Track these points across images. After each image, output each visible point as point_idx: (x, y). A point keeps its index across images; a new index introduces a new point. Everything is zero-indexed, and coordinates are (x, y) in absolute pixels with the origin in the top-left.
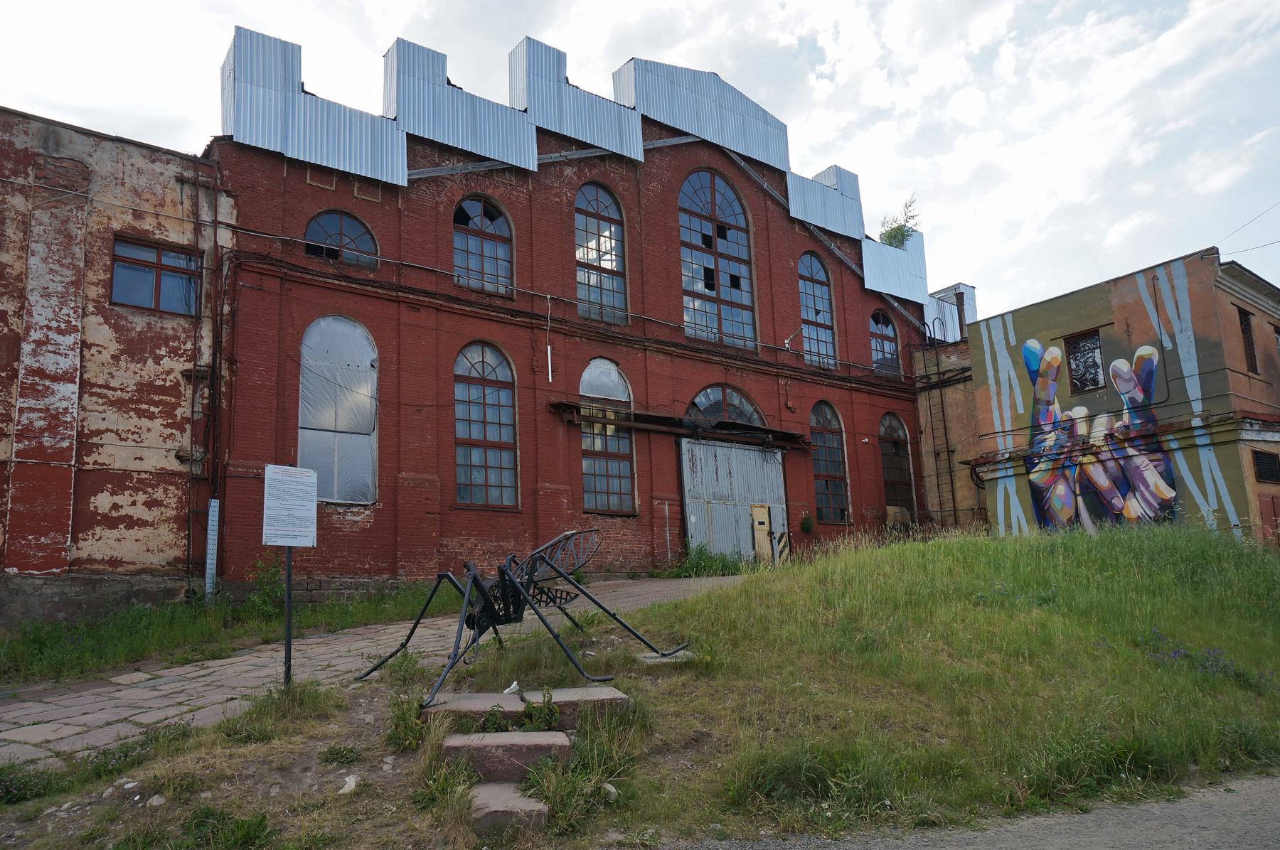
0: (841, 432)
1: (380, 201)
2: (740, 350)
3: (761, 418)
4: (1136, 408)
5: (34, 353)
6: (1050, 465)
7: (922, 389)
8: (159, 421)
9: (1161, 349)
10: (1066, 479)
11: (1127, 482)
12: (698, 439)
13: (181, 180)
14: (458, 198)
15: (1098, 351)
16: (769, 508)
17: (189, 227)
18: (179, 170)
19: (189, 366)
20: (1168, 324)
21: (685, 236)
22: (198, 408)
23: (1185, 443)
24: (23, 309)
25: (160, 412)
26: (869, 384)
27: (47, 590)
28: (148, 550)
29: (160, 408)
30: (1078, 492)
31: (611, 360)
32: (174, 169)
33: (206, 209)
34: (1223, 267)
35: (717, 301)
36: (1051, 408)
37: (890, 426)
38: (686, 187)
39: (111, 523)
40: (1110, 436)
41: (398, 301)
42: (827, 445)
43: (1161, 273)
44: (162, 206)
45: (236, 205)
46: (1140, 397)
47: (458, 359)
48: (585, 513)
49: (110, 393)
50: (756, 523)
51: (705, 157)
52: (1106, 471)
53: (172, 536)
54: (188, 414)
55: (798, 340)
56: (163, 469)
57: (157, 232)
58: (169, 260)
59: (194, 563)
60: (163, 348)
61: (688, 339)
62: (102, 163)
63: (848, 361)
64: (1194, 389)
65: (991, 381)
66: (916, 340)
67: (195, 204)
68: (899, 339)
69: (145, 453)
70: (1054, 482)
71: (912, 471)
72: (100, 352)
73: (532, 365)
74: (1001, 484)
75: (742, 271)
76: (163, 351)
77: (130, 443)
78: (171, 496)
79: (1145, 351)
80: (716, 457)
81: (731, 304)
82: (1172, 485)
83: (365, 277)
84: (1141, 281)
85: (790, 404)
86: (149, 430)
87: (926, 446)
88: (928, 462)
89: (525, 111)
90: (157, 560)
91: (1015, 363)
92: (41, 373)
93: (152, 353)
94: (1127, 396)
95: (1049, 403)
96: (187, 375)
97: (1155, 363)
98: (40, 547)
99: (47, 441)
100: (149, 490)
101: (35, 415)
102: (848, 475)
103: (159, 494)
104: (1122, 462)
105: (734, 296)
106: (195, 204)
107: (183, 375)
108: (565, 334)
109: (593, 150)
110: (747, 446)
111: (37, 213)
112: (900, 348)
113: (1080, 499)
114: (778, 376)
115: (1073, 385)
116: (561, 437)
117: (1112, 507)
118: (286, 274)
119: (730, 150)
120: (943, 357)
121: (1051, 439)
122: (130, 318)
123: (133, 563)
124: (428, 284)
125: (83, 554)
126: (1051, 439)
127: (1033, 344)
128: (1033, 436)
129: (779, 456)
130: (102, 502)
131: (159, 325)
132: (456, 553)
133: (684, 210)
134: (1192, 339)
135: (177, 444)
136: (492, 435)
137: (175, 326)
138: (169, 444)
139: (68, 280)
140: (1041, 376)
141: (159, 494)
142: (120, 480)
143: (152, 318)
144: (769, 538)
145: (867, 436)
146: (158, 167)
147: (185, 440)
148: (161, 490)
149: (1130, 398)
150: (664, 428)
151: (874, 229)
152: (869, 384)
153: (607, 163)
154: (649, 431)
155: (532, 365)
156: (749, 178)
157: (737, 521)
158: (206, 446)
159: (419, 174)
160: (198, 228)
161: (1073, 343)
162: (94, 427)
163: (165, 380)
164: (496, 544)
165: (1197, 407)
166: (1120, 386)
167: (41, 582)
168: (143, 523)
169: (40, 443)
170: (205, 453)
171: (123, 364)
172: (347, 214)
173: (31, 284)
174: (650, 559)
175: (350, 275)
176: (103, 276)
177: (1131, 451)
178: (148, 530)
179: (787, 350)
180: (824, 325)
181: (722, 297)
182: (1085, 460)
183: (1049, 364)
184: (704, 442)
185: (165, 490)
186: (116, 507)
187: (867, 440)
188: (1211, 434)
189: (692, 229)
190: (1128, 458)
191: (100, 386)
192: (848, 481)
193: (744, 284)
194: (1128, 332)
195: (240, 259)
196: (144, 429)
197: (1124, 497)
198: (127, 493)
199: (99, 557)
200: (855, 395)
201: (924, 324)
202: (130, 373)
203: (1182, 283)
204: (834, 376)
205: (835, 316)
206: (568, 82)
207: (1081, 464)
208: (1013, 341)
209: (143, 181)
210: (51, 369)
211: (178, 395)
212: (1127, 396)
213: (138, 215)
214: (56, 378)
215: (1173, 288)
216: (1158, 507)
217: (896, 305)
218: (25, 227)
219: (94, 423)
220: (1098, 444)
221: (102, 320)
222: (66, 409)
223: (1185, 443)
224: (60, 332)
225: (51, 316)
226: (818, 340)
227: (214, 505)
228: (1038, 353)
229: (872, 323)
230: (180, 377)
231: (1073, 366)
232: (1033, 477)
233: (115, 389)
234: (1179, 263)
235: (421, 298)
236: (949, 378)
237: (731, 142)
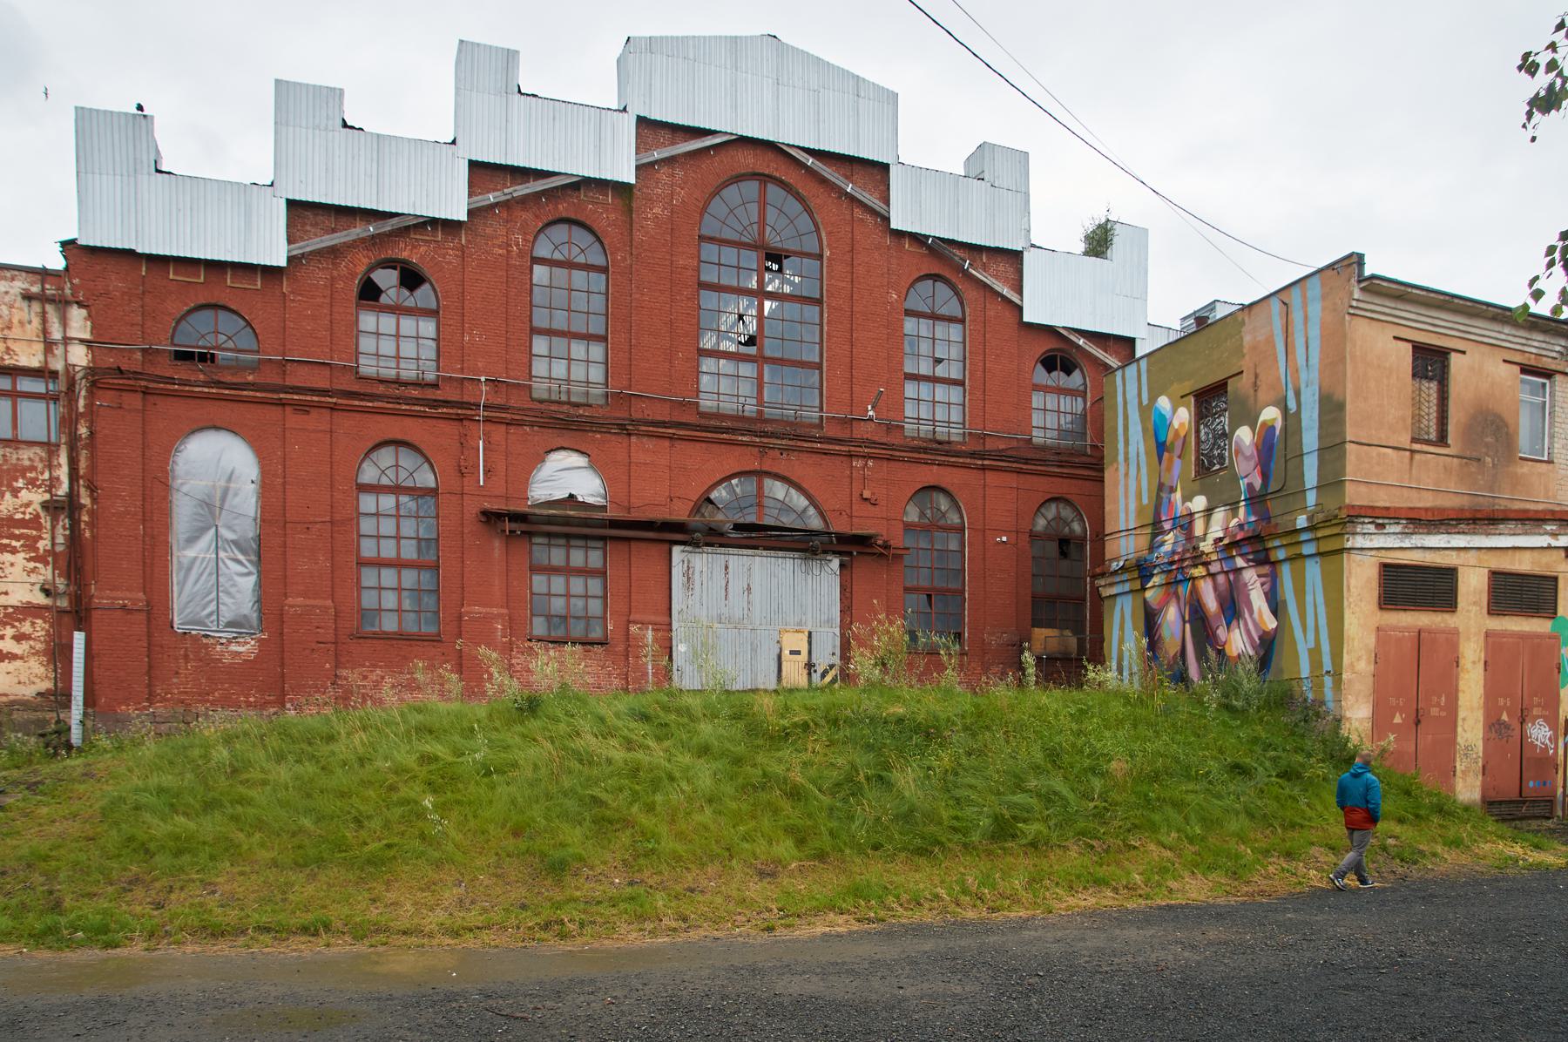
1: (259, 287)
2: (791, 424)
3: (821, 514)
8: (22, 555)
12: (699, 547)
13: (28, 297)
14: (362, 269)
16: (810, 633)
17: (40, 347)
19: (47, 497)
22: (60, 540)
23: (1293, 551)
25: (22, 546)
26: (1017, 460)
28: (19, 683)
29: (22, 542)
30: (1187, 618)
32: (19, 285)
33: (55, 320)
34: (1362, 285)
37: (1058, 518)
41: (282, 404)
42: (936, 547)
44: (9, 328)
45: (90, 317)
47: (365, 465)
50: (786, 652)
51: (748, 160)
53: (43, 669)
54: (49, 547)
56: (29, 603)
57: (6, 357)
58: (26, 385)
59: (59, 697)
60: (21, 480)
67: (44, 321)
76: (20, 484)
78: (38, 628)
79: (1270, 414)
80: (727, 568)
82: (1275, 612)
83: (242, 381)
85: (867, 494)
86: (12, 565)
89: (454, 142)
90: (28, 692)
91: (1145, 430)
93: (10, 486)
94: (1246, 481)
95: (1172, 490)
96: (45, 506)
100: (17, 624)
103: (26, 628)
106: (44, 321)
107: (43, 507)
108: (507, 424)
110: (780, 553)
113: (1188, 626)
115: (1199, 463)
116: (496, 550)
118: (147, 388)
119: (788, 145)
124: (320, 380)
128: (1154, 535)
129: (835, 563)
131: (15, 456)
132: (358, 686)
134: (1317, 397)
135: (42, 578)
137: (32, 456)
138: (33, 578)
140: (1168, 451)
141: (26, 628)
143: (8, 450)
144: (806, 672)
145: (1005, 532)
148: (28, 624)
152: (1017, 460)
153: (582, 191)
156: (823, 181)
157: (754, 650)
158: (68, 577)
159: (300, 248)
160: (49, 346)
163: (24, 513)
164: (408, 676)
168: (12, 657)
170: (67, 585)
175: (222, 380)
177: (1240, 562)
178: (18, 663)
179: (871, 419)
180: (949, 379)
181: (768, 353)
185: (33, 624)
187: (1004, 539)
188: (1318, 539)
194: (1255, 385)
195: (95, 376)
196: (7, 564)
197: (1228, 625)
200: (990, 475)
204: (960, 452)
206: (519, 91)
207: (1194, 578)
211: (39, 527)
212: (1246, 481)
215: (1306, 318)
216: (1258, 641)
223: (1293, 551)
227: (79, 638)
229: (1040, 369)
230: (39, 510)
235: (309, 398)
237: (794, 132)
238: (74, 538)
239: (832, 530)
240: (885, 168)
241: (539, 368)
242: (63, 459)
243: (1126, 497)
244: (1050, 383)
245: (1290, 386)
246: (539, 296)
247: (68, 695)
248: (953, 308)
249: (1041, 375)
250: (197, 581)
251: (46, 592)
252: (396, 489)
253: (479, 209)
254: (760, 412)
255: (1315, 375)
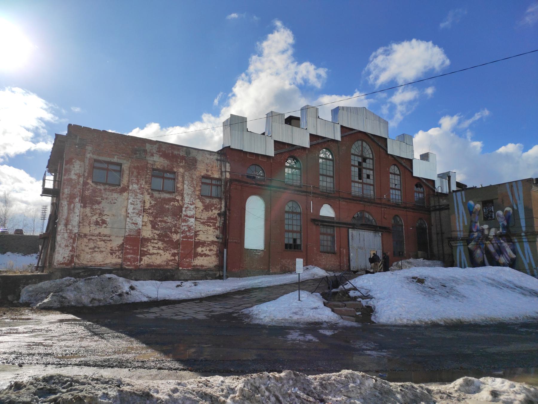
0: (403, 226)
4: (504, 227)
5: (185, 211)
6: (475, 243)
7: (433, 211)
8: (212, 227)
9: (513, 209)
10: (481, 248)
11: (500, 251)
13: (217, 160)
15: (493, 207)
18: (217, 157)
19: (219, 212)
20: (516, 201)
21: (353, 163)
24: (183, 199)
27: (189, 273)
31: (329, 204)
35: (363, 183)
36: (476, 224)
38: (354, 147)
39: (201, 255)
40: (495, 236)
43: (514, 184)
46: (505, 224)
48: (321, 252)
49: (201, 220)
52: (494, 246)
55: (389, 195)
61: (353, 196)
62: (199, 158)
63: (406, 201)
64: (523, 223)
65: (456, 213)
66: (432, 193)
67: (221, 166)
68: (425, 192)
69: (209, 236)
70: (477, 249)
71: (428, 239)
72: (199, 209)
73: (306, 207)
74: (458, 247)
75: (371, 172)
76: (213, 208)
77: (206, 234)
78: (215, 248)
79: (508, 209)
81: (367, 184)
84: (507, 186)
85: (385, 217)
87: (434, 231)
88: (434, 237)
90: (212, 266)
91: (465, 208)
92: (187, 216)
93: (211, 209)
94: (501, 223)
95: (476, 222)
96: (219, 214)
97: (511, 213)
98: (187, 262)
99: (188, 234)
101: (185, 227)
102: (404, 240)
103: (212, 248)
104: (499, 244)
105: (368, 181)
106: (221, 166)
109: (325, 139)
110: (370, 231)
111: (186, 173)
112: (425, 195)
113: (485, 255)
114: (381, 207)
117: (495, 259)
120: (441, 200)
121: (476, 234)
122: (206, 199)
123: (206, 266)
125: (195, 264)
126: (476, 234)
127: (471, 202)
129: (380, 234)
130: (199, 250)
133: (353, 154)
134: (523, 207)
136: (295, 229)
139: (192, 190)
140: (474, 213)
142: (203, 244)
146: (212, 157)
147: (218, 232)
149: (502, 224)
150: (345, 226)
151: (417, 156)
154: (340, 227)
155: (306, 207)
161: (485, 204)
162: (198, 230)
163: (213, 216)
165: (524, 229)
166: (499, 219)
167: (187, 271)
168: (208, 255)
169: (186, 234)
171: (204, 212)
172: (258, 165)
173: (185, 192)
174: (339, 267)
176: (199, 188)
177: (502, 241)
178: (209, 257)
181: (364, 182)
182: (487, 242)
183: (476, 210)
184: (356, 230)
185: (213, 246)
186: (202, 251)
189: (355, 160)
190: (501, 243)
191: (199, 218)
192: (405, 242)
193: (371, 177)
195: (231, 180)
197: (499, 256)
198: (205, 247)
199: (198, 265)
201: (435, 188)
202: (206, 215)
203: (521, 189)
205: (402, 186)
206: (319, 118)
208: (464, 201)
209: (208, 161)
210: (189, 215)
211: (216, 220)
212: (501, 223)
213: (207, 171)
214: (190, 217)
215: (518, 190)
217: (424, 181)
218: (183, 177)
219: (198, 229)
220: (491, 238)
221: (199, 200)
222: (192, 225)
224: (191, 204)
225: (189, 200)
226: (395, 194)
227: (225, 250)
228: (473, 205)
229: (415, 187)
231: (485, 211)
232: (469, 246)
233: (202, 219)
234: (520, 181)
236: (443, 208)
238: (224, 224)
239: (378, 225)
240: (386, 139)
241: (321, 183)
242: (223, 202)
243: (459, 223)
244: (417, 190)
245: (514, 203)
246: (321, 167)
247: (223, 267)
248: (398, 172)
249: (415, 189)
250: (460, 251)
251: (217, 238)
252: (293, 212)
253: (313, 145)
254: (363, 196)
255: (522, 201)
